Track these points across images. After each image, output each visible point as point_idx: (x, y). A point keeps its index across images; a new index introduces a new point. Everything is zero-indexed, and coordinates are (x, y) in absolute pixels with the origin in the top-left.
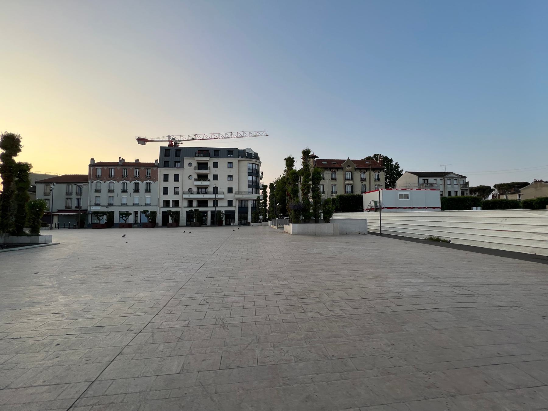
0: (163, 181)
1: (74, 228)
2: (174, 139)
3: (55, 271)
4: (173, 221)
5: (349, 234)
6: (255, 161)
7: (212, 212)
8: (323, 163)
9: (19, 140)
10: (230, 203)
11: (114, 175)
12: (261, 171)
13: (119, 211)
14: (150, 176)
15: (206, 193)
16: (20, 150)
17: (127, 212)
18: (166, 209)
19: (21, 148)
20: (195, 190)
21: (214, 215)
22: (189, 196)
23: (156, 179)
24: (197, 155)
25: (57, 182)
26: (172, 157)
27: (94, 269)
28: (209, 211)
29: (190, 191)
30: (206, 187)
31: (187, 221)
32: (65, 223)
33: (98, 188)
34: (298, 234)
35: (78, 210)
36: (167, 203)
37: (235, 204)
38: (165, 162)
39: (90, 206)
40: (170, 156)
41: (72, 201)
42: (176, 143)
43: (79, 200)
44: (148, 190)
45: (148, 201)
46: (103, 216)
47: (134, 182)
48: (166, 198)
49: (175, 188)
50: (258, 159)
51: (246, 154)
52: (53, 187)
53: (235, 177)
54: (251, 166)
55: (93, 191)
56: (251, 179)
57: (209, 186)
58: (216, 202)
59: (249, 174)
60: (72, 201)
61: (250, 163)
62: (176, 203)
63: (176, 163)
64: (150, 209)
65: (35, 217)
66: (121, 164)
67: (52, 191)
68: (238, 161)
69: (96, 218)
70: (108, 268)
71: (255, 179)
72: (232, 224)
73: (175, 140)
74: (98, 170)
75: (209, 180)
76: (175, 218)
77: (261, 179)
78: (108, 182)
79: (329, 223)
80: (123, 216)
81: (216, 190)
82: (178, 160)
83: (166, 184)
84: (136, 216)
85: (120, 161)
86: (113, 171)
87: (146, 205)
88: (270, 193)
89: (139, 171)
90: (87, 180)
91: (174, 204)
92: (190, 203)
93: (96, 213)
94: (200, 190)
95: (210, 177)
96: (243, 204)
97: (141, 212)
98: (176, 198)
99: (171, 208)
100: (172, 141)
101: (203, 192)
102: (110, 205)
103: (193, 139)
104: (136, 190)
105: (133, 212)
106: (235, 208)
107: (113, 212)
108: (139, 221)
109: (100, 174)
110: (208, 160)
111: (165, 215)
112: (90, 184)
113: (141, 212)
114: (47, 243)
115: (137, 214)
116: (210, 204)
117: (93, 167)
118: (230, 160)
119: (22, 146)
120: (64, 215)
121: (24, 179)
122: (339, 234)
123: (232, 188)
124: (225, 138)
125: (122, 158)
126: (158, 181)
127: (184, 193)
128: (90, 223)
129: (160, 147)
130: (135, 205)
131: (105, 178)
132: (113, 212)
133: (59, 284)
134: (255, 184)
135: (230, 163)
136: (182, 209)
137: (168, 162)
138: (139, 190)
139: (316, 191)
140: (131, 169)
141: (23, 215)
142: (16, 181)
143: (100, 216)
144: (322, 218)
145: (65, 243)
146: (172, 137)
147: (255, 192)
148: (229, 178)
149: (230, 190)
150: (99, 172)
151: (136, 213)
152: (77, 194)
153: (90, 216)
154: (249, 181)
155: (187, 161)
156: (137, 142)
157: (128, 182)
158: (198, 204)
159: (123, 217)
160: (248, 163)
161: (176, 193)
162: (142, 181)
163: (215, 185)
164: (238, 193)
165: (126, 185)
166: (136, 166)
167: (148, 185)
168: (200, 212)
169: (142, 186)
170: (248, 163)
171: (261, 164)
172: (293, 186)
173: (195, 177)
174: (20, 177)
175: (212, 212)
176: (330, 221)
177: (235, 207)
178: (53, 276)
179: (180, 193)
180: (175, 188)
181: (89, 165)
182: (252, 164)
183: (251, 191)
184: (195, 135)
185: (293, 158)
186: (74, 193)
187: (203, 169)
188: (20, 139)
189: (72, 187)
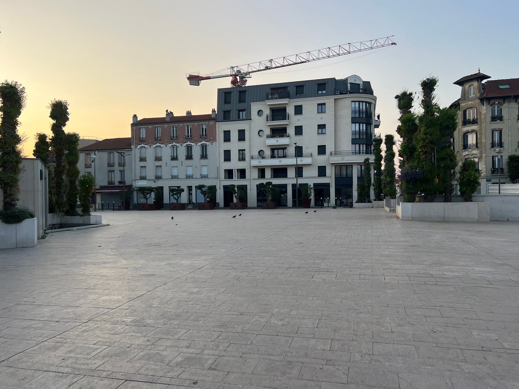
0: (223, 140)
1: (119, 210)
2: (239, 71)
3: (114, 246)
4: (238, 200)
5: (513, 221)
6: (364, 97)
7: (294, 186)
8: (501, 87)
9: (66, 107)
10: (322, 171)
11: (161, 136)
12: (377, 113)
13: (169, 187)
14: (206, 135)
15: (285, 156)
16: (68, 119)
17: (178, 187)
18: (229, 183)
19: (68, 117)
20: (268, 152)
21: (296, 190)
22: (260, 162)
23: (214, 139)
24: (270, 97)
25: (99, 150)
26: (234, 105)
27: (146, 245)
28: (289, 184)
29: (261, 154)
30: (284, 148)
31: (258, 200)
32: (114, 203)
33: (143, 156)
34: (413, 219)
35: (122, 186)
36: (229, 174)
37: (330, 172)
38: (225, 112)
39: (135, 180)
40: (232, 102)
41: (114, 174)
42: (242, 78)
43: (122, 172)
44: (204, 156)
45: (205, 172)
46: (150, 193)
47: (186, 145)
48: (228, 166)
49: (239, 150)
50: (371, 93)
51: (349, 85)
52: (95, 157)
53: (330, 129)
54: (357, 105)
55: (138, 159)
56: (357, 129)
57: (288, 145)
58: (299, 171)
59: (354, 121)
60: (114, 174)
61: (355, 102)
62: (242, 173)
63: (241, 113)
64: (208, 183)
65: (85, 194)
66: (168, 120)
67: (94, 162)
68: (335, 100)
69: (142, 196)
70: (158, 245)
71: (364, 128)
72: (325, 204)
73: (240, 72)
74: (141, 130)
75: (289, 136)
76: (239, 195)
77: (377, 126)
78: (154, 146)
79: (471, 201)
80: (174, 193)
81: (299, 152)
82: (243, 108)
83: (227, 146)
84: (190, 194)
85: (168, 116)
86: (159, 130)
87: (203, 177)
88: (386, 152)
89: (191, 127)
90: (130, 145)
91: (239, 175)
92: (262, 172)
93: (143, 190)
94: (276, 151)
95: (291, 131)
96: (344, 172)
97: (196, 187)
98: (241, 165)
99: (236, 182)
100: (236, 75)
101: (279, 156)
102: (158, 178)
103: (267, 68)
104: (189, 157)
105: (186, 187)
106: (330, 179)
107: (162, 188)
108: (194, 201)
109: (144, 136)
110: (287, 104)
111: (228, 191)
112: (133, 151)
113: (196, 187)
114: (98, 225)
115: (192, 190)
116: (291, 173)
117: (136, 127)
118: (321, 100)
119: (69, 113)
120: (108, 193)
121: (73, 152)
122: (489, 221)
123: (325, 146)
124: (318, 59)
125: (169, 111)
126: (216, 141)
127: (252, 158)
128: (136, 203)
129: (218, 89)
130: (188, 177)
131: (150, 141)
132: (162, 188)
133: (120, 253)
134: (364, 137)
135: (322, 105)
136: (250, 182)
137: (230, 111)
138: (193, 156)
139: (445, 148)
140: (181, 126)
141: (75, 193)
142: (66, 154)
143: (147, 194)
144: (459, 193)
145: (113, 225)
146: (235, 69)
147: (364, 151)
148: (320, 130)
149: (322, 150)
150: (143, 133)
151: (190, 188)
152: (120, 165)
153: (135, 193)
154: (354, 133)
155: (255, 107)
156: (188, 82)
157: (178, 145)
158: (260, 174)
159: (174, 196)
160: (352, 101)
161: (242, 158)
162: (196, 142)
163: (296, 144)
164: (336, 153)
165: (176, 149)
166: (188, 121)
167: (204, 148)
168: (275, 186)
169: (197, 150)
170: (352, 101)
171: (375, 100)
172: (407, 141)
173: (268, 132)
174: (70, 150)
175: (294, 186)
176: (473, 198)
177: (331, 177)
178: (114, 249)
179: (247, 157)
180: (239, 150)
181: (131, 124)
182: (359, 102)
183: (357, 149)
184: (269, 61)
185: (411, 94)
186: (116, 164)
187: (279, 118)
188: (67, 106)
189: (114, 156)
